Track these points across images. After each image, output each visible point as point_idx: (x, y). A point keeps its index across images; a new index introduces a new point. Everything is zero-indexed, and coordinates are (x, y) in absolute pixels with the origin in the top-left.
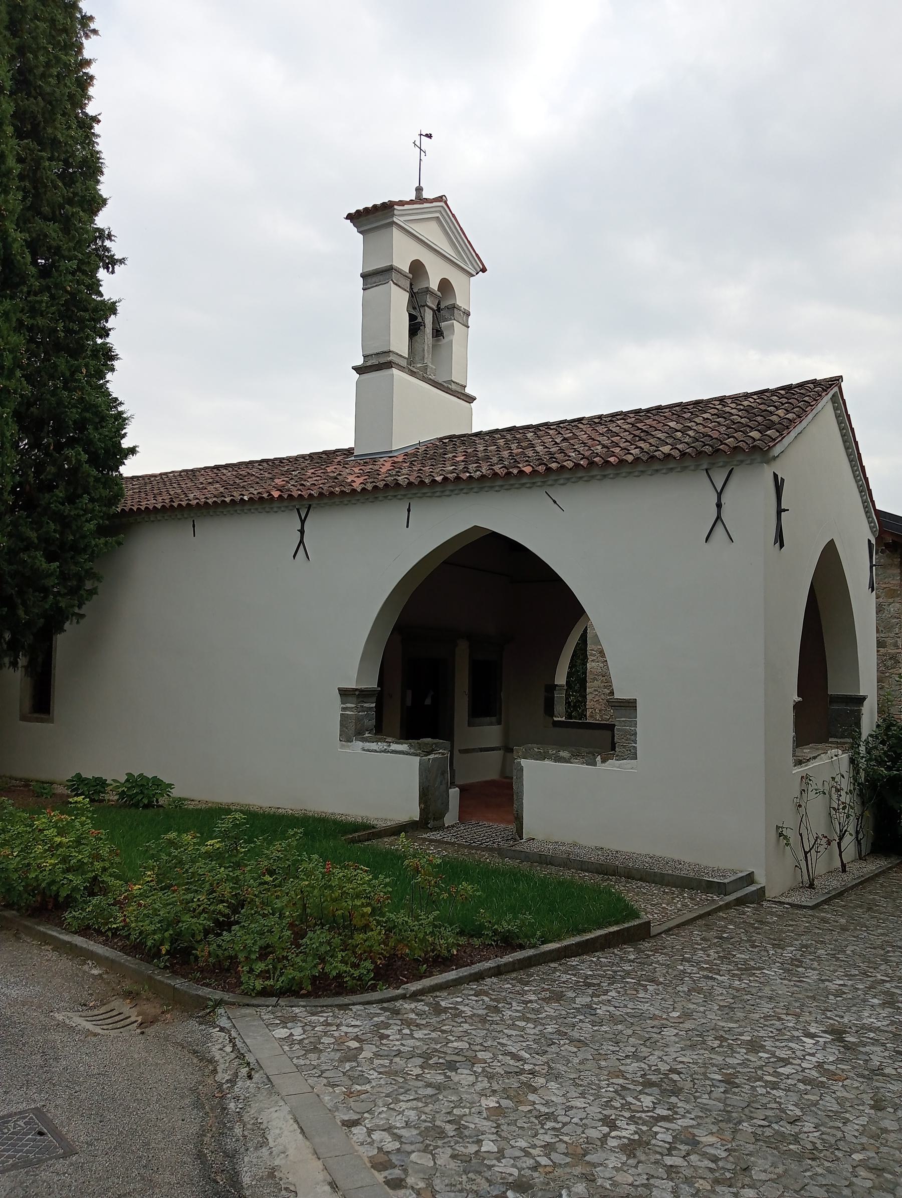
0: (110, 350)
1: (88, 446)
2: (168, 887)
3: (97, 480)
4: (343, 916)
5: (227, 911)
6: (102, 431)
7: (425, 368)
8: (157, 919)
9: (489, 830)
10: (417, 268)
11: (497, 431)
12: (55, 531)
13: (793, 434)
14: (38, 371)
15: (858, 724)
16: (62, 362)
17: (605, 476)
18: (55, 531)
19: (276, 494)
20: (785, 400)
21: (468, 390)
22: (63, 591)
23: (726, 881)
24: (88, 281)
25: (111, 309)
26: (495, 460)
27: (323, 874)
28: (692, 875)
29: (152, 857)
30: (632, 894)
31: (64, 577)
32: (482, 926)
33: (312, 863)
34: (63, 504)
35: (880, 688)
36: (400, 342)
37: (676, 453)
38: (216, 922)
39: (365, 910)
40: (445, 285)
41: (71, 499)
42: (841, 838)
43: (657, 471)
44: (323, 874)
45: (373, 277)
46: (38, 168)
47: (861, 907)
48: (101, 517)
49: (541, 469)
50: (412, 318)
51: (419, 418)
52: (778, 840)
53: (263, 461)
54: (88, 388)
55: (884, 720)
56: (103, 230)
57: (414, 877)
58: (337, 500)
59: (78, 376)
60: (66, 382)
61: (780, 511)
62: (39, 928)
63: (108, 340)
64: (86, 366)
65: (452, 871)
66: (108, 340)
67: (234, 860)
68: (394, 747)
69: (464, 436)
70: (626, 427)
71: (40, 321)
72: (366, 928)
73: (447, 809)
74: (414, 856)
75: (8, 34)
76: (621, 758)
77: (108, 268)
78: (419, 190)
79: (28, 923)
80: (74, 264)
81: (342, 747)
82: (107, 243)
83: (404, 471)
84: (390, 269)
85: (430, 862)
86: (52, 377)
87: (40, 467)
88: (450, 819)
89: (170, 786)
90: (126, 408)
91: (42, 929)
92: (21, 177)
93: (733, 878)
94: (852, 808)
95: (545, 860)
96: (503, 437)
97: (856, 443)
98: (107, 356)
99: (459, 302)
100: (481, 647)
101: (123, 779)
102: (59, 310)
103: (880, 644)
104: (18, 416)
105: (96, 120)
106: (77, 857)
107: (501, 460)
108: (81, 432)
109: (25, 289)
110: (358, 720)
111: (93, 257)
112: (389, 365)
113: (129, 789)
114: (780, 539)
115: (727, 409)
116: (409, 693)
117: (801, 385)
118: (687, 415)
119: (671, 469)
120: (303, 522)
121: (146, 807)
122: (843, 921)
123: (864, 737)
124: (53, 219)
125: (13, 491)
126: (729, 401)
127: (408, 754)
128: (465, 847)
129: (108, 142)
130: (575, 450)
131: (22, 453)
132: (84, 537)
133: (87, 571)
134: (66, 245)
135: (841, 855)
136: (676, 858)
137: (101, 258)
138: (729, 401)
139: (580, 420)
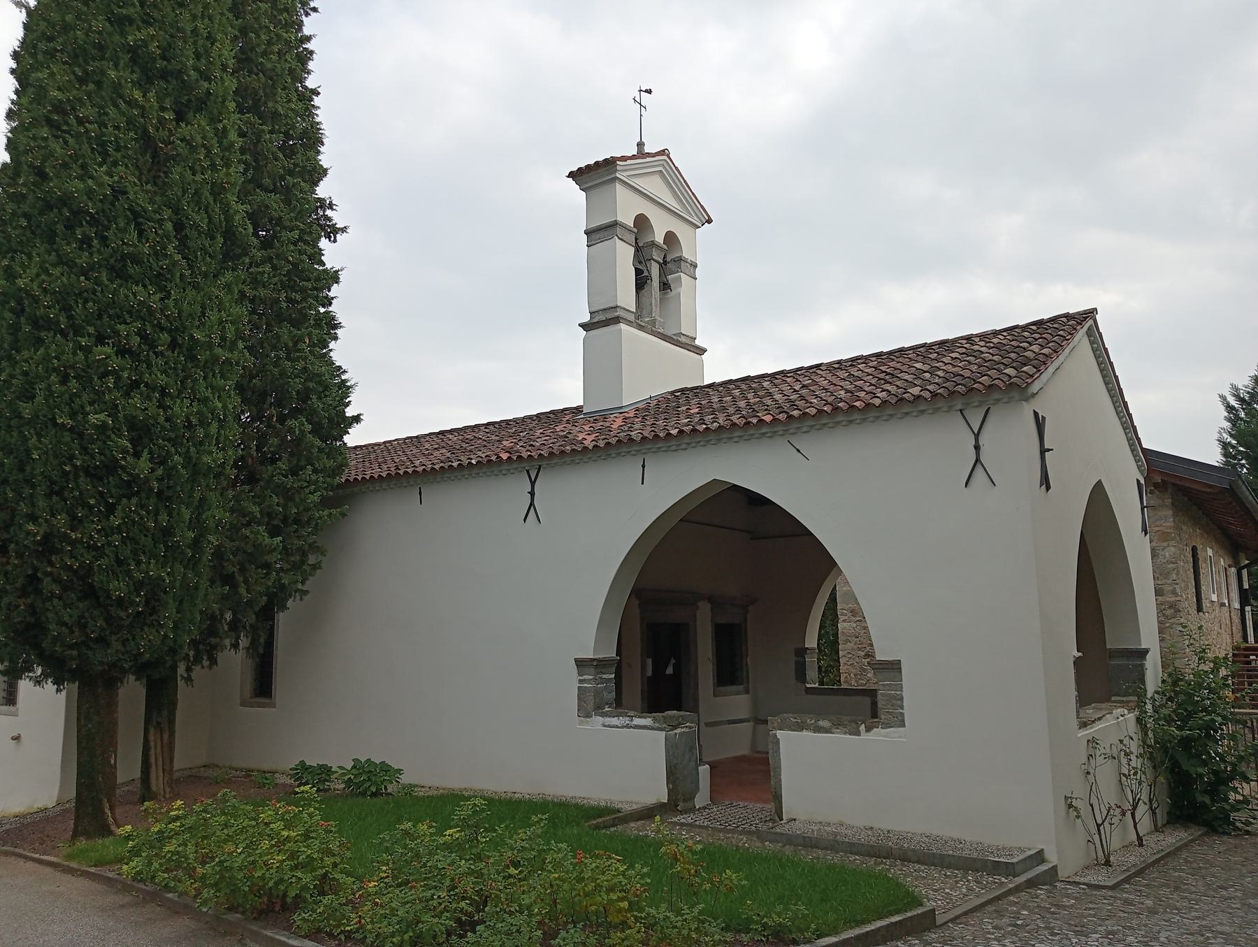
0: (333, 318)
1: (311, 416)
2: (406, 883)
3: (321, 450)
4: (597, 913)
5: (470, 909)
6: (326, 399)
7: (654, 322)
8: (395, 919)
9: (749, 811)
10: (641, 221)
11: (730, 382)
12: (278, 505)
13: (1051, 370)
14: (261, 342)
15: (1142, 680)
16: (285, 332)
17: (851, 422)
18: (278, 505)
19: (505, 456)
20: (1037, 336)
21: (697, 342)
22: (286, 566)
23: (1014, 860)
24: (309, 250)
25: (333, 277)
26: (732, 410)
27: (574, 865)
28: (975, 855)
29: (387, 850)
30: (910, 877)
31: (286, 552)
32: (749, 920)
33: (560, 851)
34: (286, 476)
35: (1162, 640)
36: (626, 297)
37: (927, 395)
38: (458, 921)
39: (622, 905)
40: (671, 238)
41: (294, 472)
42: (1135, 807)
43: (907, 414)
44: (574, 865)
45: (595, 234)
46: (259, 141)
47: (1167, 886)
48: (325, 489)
49: (782, 417)
50: (638, 272)
51: (649, 371)
52: (1068, 813)
53: (489, 424)
54: (311, 357)
55: (1170, 675)
56: (324, 200)
57: (672, 866)
58: (568, 459)
59: (301, 346)
60: (288, 354)
61: (1043, 451)
62: (265, 932)
63: (330, 309)
64: (310, 335)
65: (713, 858)
66: (330, 309)
67: (474, 851)
68: (637, 721)
69: (697, 388)
70: (869, 370)
71: (262, 292)
72: (624, 925)
73: (697, 789)
74: (671, 842)
75: (230, 15)
76: (887, 725)
77: (329, 238)
78: (640, 145)
79: (254, 928)
80: (296, 234)
81: (581, 723)
82: (329, 212)
83: (636, 426)
84: (615, 224)
85: (690, 850)
86: (274, 348)
87: (262, 439)
88: (702, 799)
89: (399, 771)
90: (350, 376)
91: (269, 933)
92: (243, 150)
93: (1021, 857)
94: (1144, 773)
95: (810, 843)
96: (738, 387)
97: (1116, 377)
98: (330, 326)
99: (685, 255)
100: (725, 610)
101: (349, 765)
102: (281, 281)
103: (1158, 592)
104: (240, 388)
105: (316, 92)
106: (305, 852)
107: (739, 410)
108: (305, 402)
109: (247, 261)
110: (597, 693)
111: (315, 227)
112: (617, 320)
113: (356, 776)
114: (1045, 481)
115: (976, 347)
116: (649, 661)
117: (1054, 320)
118: (934, 356)
119: (922, 412)
120: (533, 483)
121: (374, 795)
122: (1149, 902)
123: (1149, 695)
124: (274, 191)
125: (235, 466)
126: (977, 340)
127: (652, 729)
128: (720, 831)
129: (326, 113)
130: (817, 396)
131: (245, 426)
132: (307, 510)
133: (310, 545)
134: (287, 217)
135: (1137, 831)
136: (956, 836)
137: (322, 227)
138: (977, 340)
139: (818, 366)
